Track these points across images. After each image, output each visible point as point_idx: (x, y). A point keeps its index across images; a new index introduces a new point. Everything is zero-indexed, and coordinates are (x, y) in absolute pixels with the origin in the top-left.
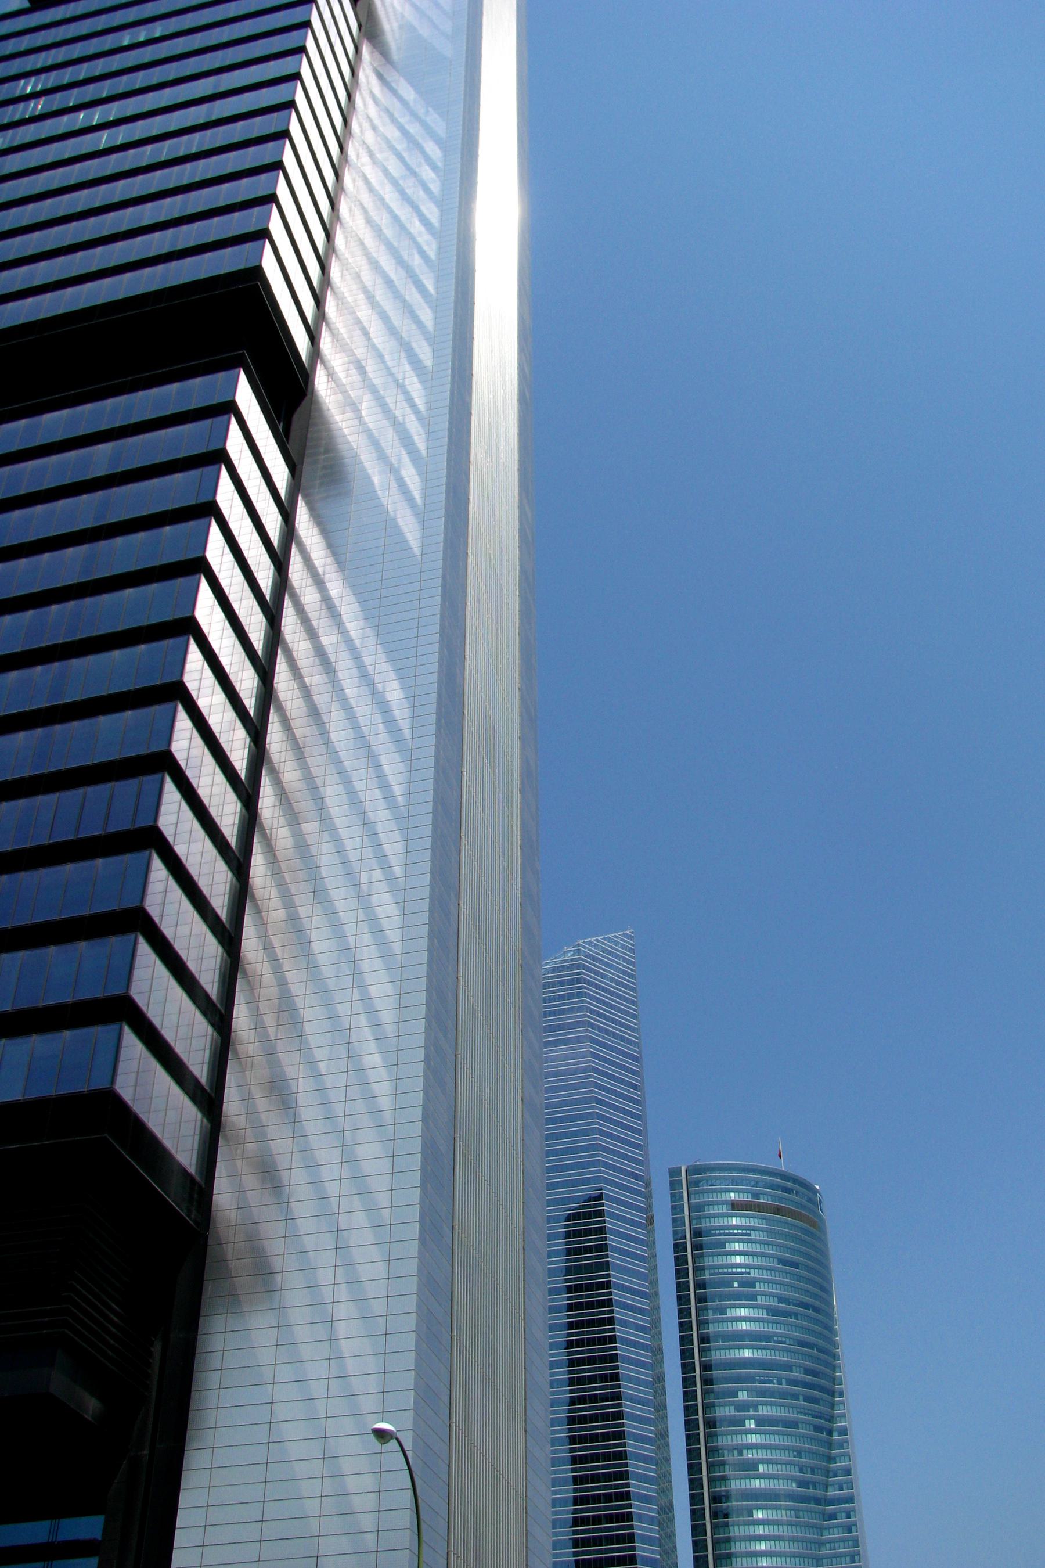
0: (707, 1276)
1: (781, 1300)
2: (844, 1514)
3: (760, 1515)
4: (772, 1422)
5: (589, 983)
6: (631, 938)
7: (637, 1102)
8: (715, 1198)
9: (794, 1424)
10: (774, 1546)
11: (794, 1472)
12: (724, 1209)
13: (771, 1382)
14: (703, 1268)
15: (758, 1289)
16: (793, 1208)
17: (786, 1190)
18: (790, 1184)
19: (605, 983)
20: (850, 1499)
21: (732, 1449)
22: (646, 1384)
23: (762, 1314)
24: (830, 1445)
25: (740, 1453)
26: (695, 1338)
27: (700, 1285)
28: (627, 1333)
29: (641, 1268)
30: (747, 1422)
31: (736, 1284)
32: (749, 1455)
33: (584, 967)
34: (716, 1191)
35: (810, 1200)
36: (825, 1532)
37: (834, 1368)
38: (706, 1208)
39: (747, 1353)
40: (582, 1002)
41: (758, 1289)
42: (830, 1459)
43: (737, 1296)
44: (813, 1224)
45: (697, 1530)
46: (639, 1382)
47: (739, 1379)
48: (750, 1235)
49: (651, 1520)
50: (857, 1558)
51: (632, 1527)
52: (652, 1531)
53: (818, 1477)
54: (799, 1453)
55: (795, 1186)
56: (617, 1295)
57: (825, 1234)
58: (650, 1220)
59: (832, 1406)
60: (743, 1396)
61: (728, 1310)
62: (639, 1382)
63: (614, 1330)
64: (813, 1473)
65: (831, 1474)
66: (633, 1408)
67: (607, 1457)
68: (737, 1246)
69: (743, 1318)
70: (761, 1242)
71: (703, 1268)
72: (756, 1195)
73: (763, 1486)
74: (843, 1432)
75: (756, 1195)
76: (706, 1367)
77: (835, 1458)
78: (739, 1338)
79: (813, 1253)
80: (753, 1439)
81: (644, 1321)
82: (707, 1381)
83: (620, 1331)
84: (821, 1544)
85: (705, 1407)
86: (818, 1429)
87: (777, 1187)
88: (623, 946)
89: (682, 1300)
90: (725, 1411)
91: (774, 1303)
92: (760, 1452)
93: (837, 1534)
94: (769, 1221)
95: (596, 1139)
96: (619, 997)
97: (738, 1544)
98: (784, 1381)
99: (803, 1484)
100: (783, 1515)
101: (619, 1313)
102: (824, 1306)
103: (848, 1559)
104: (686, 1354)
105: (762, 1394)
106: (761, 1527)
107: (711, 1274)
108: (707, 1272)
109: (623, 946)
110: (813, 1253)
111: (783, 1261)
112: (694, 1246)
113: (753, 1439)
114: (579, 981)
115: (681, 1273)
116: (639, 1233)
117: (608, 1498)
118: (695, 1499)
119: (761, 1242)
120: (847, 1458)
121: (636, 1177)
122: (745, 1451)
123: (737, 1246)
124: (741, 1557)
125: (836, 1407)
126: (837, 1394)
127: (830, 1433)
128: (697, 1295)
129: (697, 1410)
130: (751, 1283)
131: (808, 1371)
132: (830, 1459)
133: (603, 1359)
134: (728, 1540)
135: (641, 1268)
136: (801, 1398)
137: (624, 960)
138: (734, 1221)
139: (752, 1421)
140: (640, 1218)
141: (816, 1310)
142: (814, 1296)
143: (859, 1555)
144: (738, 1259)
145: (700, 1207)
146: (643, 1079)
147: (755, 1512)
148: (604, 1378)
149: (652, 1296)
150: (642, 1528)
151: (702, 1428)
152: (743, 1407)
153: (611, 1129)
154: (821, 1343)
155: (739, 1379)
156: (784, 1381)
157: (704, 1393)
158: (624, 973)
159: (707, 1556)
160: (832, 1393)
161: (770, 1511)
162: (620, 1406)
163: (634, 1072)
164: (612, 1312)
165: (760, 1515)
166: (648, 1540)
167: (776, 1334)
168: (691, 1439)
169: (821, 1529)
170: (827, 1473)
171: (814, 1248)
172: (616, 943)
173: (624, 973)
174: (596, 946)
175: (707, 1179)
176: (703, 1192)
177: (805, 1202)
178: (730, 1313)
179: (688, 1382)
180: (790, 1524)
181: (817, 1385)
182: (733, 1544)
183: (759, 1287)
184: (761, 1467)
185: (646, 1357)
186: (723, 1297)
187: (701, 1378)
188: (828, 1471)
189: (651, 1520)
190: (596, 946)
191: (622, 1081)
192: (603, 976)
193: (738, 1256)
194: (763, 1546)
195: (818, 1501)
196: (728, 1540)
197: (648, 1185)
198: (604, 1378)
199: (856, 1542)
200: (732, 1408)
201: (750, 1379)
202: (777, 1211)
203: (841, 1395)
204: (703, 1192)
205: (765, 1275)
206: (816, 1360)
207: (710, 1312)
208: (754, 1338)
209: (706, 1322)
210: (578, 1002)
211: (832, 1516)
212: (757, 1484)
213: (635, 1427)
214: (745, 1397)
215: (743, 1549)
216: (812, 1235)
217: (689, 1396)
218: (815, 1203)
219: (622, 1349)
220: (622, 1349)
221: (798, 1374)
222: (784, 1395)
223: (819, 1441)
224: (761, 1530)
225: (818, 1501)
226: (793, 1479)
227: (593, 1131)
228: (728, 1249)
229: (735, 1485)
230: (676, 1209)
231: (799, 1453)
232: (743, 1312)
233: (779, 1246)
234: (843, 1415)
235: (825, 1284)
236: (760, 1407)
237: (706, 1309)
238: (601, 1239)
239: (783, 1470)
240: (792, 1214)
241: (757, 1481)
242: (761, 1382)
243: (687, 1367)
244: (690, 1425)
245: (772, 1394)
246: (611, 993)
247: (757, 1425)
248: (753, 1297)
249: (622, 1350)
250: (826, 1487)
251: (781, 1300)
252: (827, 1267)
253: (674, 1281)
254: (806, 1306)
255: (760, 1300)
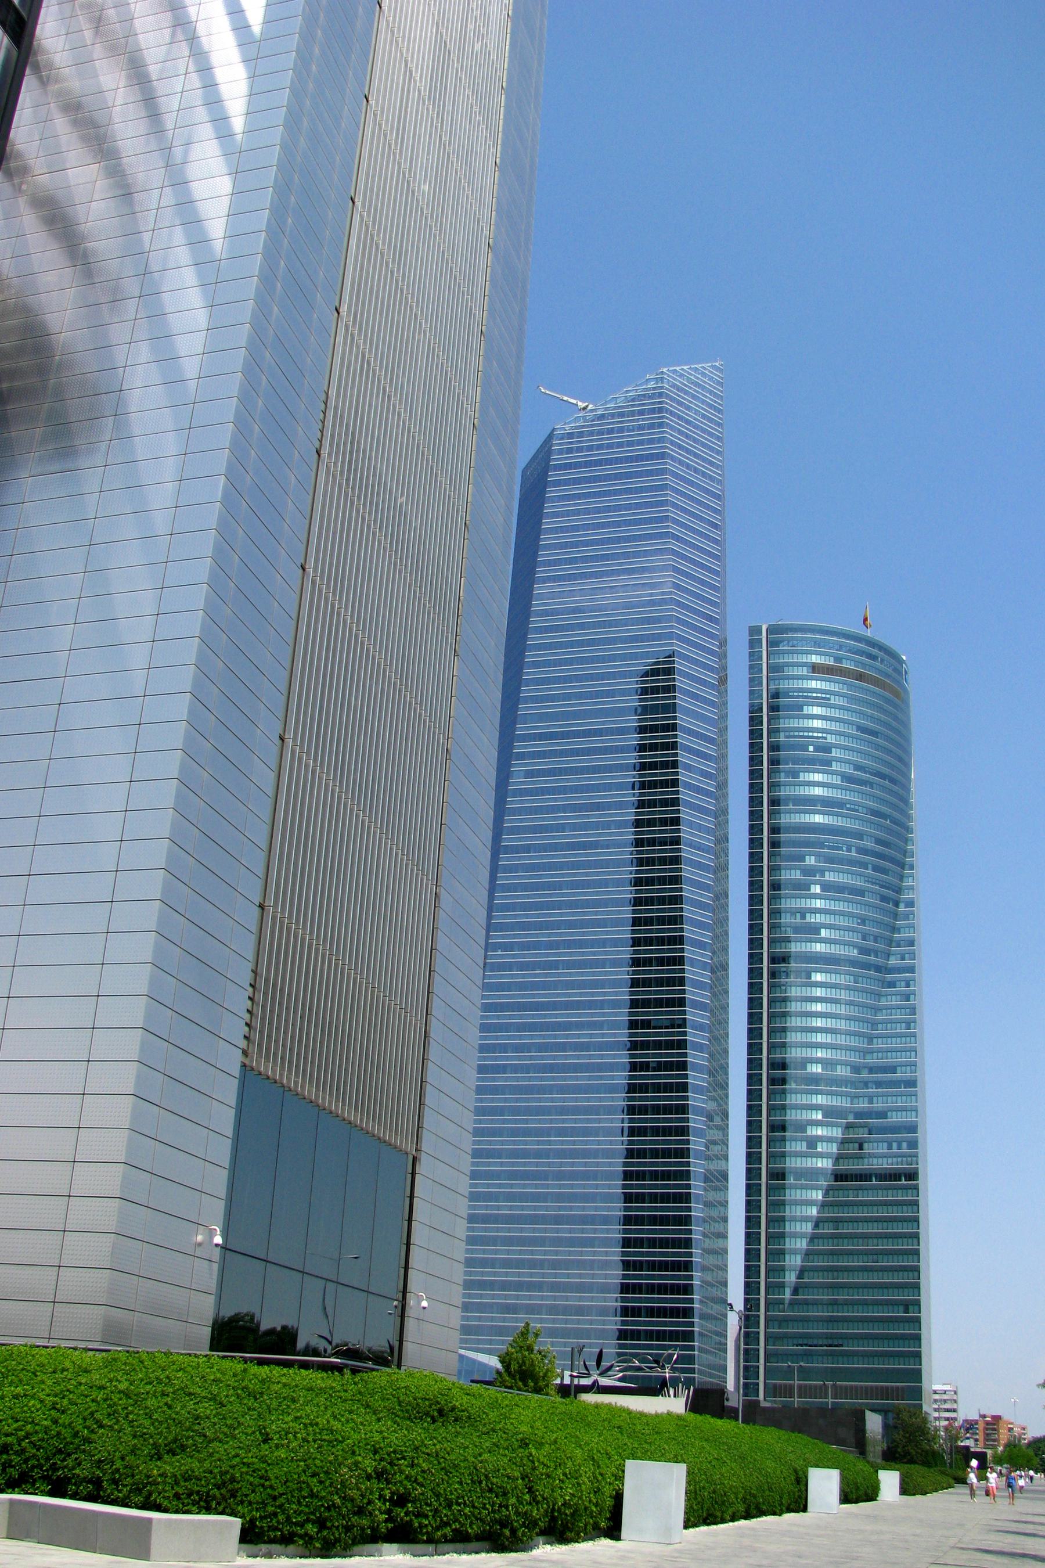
0: (782, 738)
1: (858, 767)
2: (903, 984)
3: (818, 977)
4: (840, 888)
5: (672, 413)
6: (721, 371)
7: (716, 541)
8: (796, 658)
9: (860, 892)
10: (829, 1023)
11: (856, 939)
12: (804, 671)
13: (841, 849)
14: (778, 731)
15: (819, 1149)
16: (878, 677)
17: (874, 658)
18: (875, 651)
19: (691, 416)
20: (911, 969)
21: (794, 912)
22: (707, 830)
23: (836, 780)
24: (896, 916)
25: (803, 917)
26: (765, 800)
27: (774, 747)
28: (691, 778)
29: (711, 713)
30: (812, 886)
31: (811, 748)
32: (811, 919)
33: (668, 396)
34: (798, 652)
35: (895, 670)
36: (883, 999)
37: (906, 841)
38: (786, 669)
39: (818, 819)
40: (662, 418)
41: (833, 755)
42: (894, 929)
43: (811, 761)
44: (897, 695)
45: (754, 988)
46: (700, 828)
47: (808, 844)
48: (829, 699)
49: (704, 966)
50: (912, 1025)
51: (684, 992)
52: (703, 996)
53: (881, 946)
54: (863, 921)
55: (879, 652)
56: (682, 738)
57: (908, 705)
58: (723, 680)
59: (901, 878)
60: (811, 861)
61: (801, 774)
62: (700, 828)
63: (678, 792)
64: (876, 941)
65: (894, 944)
66: (692, 854)
67: (662, 901)
68: (816, 710)
69: (816, 783)
70: (834, 942)
71: (778, 731)
72: (838, 659)
73: (823, 950)
74: (911, 904)
75: (838, 659)
76: (774, 830)
77: (899, 929)
78: (810, 803)
79: (894, 723)
80: (818, 904)
81: (710, 767)
82: (774, 844)
83: (683, 775)
84: (877, 1010)
85: (771, 869)
86: (884, 899)
87: (861, 653)
88: (711, 379)
89: (755, 761)
90: (790, 875)
91: (848, 770)
92: (824, 916)
93: (895, 1001)
94: (850, 686)
95: (672, 627)
96: (704, 445)
97: (793, 1034)
98: (853, 849)
99: (864, 951)
100: (840, 979)
101: (683, 757)
102: (899, 778)
103: (904, 1025)
104: (755, 815)
105: (830, 860)
106: (819, 989)
107: (787, 737)
108: (782, 734)
109: (711, 379)
110: (894, 723)
111: (861, 728)
112: (771, 709)
113: (818, 904)
114: (661, 395)
115: (755, 734)
116: (711, 695)
117: (661, 941)
118: (753, 1064)
119: (834, 942)
120: (912, 930)
121: (710, 618)
122: (808, 915)
123: (816, 710)
124: (797, 1001)
125: (905, 879)
126: (907, 867)
127: (897, 904)
128: (770, 755)
129: (762, 872)
130: (827, 749)
131: (879, 841)
132: (894, 929)
133: (664, 803)
134: (784, 1030)
135: (711, 713)
136: (870, 866)
137: (711, 392)
138: (814, 684)
139: (818, 887)
140: (712, 678)
141: (893, 781)
142: (892, 767)
143: (915, 1022)
144: (817, 724)
145: (776, 695)
146: (724, 519)
147: (813, 974)
148: (664, 822)
149: (722, 744)
150: (694, 973)
151: (765, 891)
152: (809, 871)
153: (698, 726)
154: (896, 815)
155: (808, 844)
156: (853, 849)
157: (770, 856)
158: (710, 406)
159: (762, 1013)
160: (902, 865)
161: (828, 975)
162: (679, 850)
163: (715, 511)
164: (676, 736)
165: (818, 977)
166: (701, 1027)
167: (850, 802)
168: (754, 900)
169: (879, 995)
170: (890, 942)
171: (896, 718)
172: (704, 375)
173: (710, 406)
174: (681, 376)
175: (789, 640)
176: (784, 652)
177: (890, 671)
178: (804, 777)
179: (755, 843)
180: (847, 988)
181: (887, 857)
182: (788, 1018)
183: (835, 753)
184: (823, 931)
185: (709, 822)
186: (796, 761)
187: (769, 841)
188: (891, 941)
189: (704, 966)
190: (681, 376)
191: (701, 519)
192: (688, 408)
193: (815, 721)
194: (818, 1007)
195: (878, 969)
196: (784, 1015)
197: (723, 643)
198: (664, 822)
199: (913, 1010)
200: (798, 872)
201: (821, 845)
202: (860, 677)
203: (912, 868)
204: (784, 652)
205: (842, 741)
206: (890, 831)
207: (783, 775)
208: (827, 804)
209: (778, 868)
210: (660, 418)
211: (892, 984)
212: (819, 947)
213: (693, 873)
214: (813, 862)
215: (799, 1040)
216: (896, 706)
217: (755, 857)
218: (900, 673)
219: (684, 793)
220: (684, 793)
221: (869, 844)
222: (851, 862)
223: (883, 910)
224: (819, 992)
225: (878, 969)
226: (854, 945)
227: (670, 618)
228: (805, 712)
229: (794, 948)
230: (754, 668)
231: (863, 921)
232: (817, 777)
233: (861, 713)
234: (912, 888)
235: (903, 756)
236: (827, 873)
237: (779, 771)
238: (669, 680)
239: (847, 936)
240: (875, 682)
241: (818, 945)
242: (829, 848)
243: (755, 829)
244: (754, 885)
245: (841, 861)
246: (696, 427)
247: (822, 890)
248: (828, 763)
249: (684, 794)
250: (888, 955)
251: (858, 767)
252: (908, 741)
253: (747, 782)
254: (882, 776)
255: (835, 766)
